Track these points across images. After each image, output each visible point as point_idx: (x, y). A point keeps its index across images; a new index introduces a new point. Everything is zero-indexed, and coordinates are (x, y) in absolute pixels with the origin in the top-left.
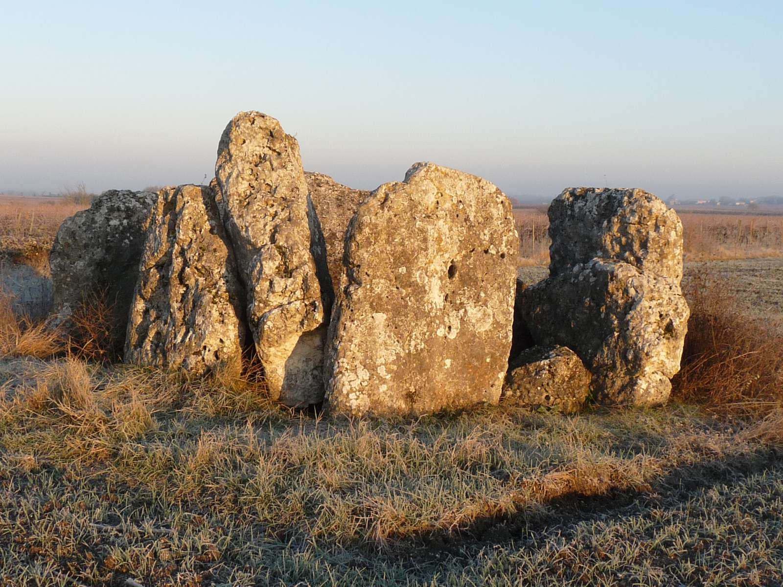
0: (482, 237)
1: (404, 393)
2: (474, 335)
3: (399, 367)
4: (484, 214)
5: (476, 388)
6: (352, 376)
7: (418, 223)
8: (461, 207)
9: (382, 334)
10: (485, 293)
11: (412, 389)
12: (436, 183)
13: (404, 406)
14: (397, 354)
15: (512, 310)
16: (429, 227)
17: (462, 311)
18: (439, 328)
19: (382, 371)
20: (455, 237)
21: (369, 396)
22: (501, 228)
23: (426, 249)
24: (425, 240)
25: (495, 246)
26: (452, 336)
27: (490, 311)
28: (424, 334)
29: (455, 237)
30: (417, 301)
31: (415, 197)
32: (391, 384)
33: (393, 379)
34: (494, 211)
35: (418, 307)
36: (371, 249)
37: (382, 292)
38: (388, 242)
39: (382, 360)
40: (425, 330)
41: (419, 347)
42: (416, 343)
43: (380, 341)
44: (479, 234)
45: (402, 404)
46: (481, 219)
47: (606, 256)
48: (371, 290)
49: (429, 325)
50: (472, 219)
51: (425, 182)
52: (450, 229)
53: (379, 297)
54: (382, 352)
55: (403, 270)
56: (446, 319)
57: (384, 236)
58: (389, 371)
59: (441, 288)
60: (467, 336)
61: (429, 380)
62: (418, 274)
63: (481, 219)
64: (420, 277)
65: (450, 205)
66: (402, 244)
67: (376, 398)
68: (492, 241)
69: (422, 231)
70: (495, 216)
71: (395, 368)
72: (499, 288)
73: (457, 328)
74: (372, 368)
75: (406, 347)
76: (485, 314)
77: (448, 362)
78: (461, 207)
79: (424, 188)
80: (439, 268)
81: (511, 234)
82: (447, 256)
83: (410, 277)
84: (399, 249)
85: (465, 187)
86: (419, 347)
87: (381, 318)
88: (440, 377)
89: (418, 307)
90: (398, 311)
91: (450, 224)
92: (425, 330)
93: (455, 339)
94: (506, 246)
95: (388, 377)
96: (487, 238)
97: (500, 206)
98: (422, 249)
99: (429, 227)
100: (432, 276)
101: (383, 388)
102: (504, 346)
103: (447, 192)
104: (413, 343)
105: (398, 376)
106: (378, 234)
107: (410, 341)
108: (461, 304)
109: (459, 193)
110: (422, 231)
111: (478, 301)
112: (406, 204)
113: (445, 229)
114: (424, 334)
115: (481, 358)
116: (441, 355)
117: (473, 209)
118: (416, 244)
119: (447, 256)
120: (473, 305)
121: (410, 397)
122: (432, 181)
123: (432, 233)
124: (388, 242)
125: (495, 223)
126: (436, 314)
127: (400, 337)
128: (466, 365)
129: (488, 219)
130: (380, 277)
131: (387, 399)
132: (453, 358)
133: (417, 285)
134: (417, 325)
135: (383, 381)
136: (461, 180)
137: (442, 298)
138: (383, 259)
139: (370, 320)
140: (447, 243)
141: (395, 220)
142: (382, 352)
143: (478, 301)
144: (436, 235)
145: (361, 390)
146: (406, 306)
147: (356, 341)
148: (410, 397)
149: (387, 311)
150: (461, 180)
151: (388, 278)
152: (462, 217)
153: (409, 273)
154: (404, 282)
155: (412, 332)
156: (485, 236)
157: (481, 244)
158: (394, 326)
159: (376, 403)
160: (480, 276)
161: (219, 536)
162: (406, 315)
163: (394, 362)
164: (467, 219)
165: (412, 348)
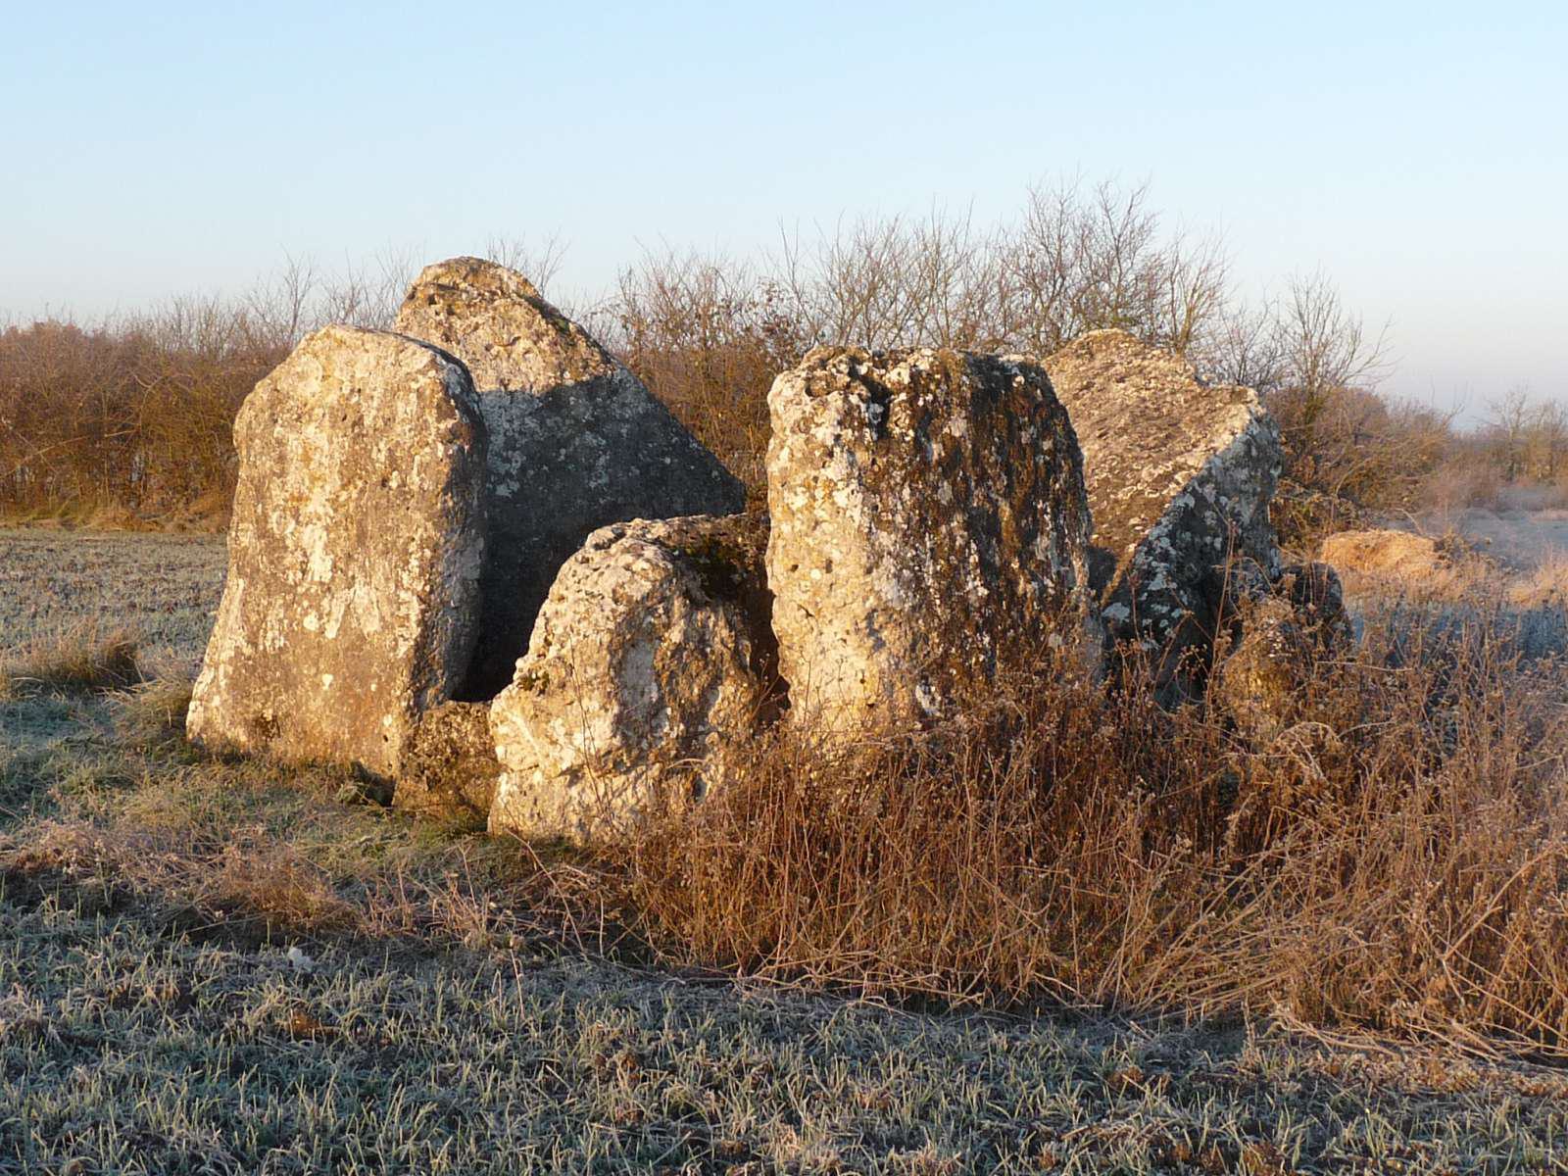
1: (251, 717)
7: (278, 429)
8: (354, 399)
11: (268, 715)
13: (243, 738)
15: (414, 610)
16: (292, 436)
18: (306, 614)
22: (407, 440)
23: (282, 474)
24: (282, 459)
30: (272, 562)
31: (283, 386)
35: (274, 575)
40: (281, 616)
44: (371, 450)
45: (241, 735)
49: (287, 606)
50: (368, 421)
56: (325, 603)
59: (326, 546)
65: (336, 397)
68: (393, 462)
69: (280, 442)
70: (400, 415)
77: (327, 679)
78: (354, 399)
79: (299, 369)
80: (321, 510)
81: (427, 450)
85: (373, 363)
88: (316, 704)
89: (274, 575)
91: (328, 430)
92: (281, 616)
93: (336, 639)
94: (419, 474)
96: (382, 457)
97: (413, 397)
98: (274, 474)
99: (292, 436)
100: (309, 522)
103: (337, 374)
104: (270, 635)
107: (266, 631)
109: (358, 375)
110: (280, 442)
113: (322, 440)
116: (316, 664)
117: (375, 404)
118: (268, 465)
121: (262, 727)
122: (315, 355)
123: (294, 447)
125: (398, 429)
126: (308, 590)
132: (334, 674)
134: (270, 603)
136: (367, 351)
137: (329, 564)
148: (262, 727)
150: (367, 351)
161: (1075, 1122)
165: (268, 644)
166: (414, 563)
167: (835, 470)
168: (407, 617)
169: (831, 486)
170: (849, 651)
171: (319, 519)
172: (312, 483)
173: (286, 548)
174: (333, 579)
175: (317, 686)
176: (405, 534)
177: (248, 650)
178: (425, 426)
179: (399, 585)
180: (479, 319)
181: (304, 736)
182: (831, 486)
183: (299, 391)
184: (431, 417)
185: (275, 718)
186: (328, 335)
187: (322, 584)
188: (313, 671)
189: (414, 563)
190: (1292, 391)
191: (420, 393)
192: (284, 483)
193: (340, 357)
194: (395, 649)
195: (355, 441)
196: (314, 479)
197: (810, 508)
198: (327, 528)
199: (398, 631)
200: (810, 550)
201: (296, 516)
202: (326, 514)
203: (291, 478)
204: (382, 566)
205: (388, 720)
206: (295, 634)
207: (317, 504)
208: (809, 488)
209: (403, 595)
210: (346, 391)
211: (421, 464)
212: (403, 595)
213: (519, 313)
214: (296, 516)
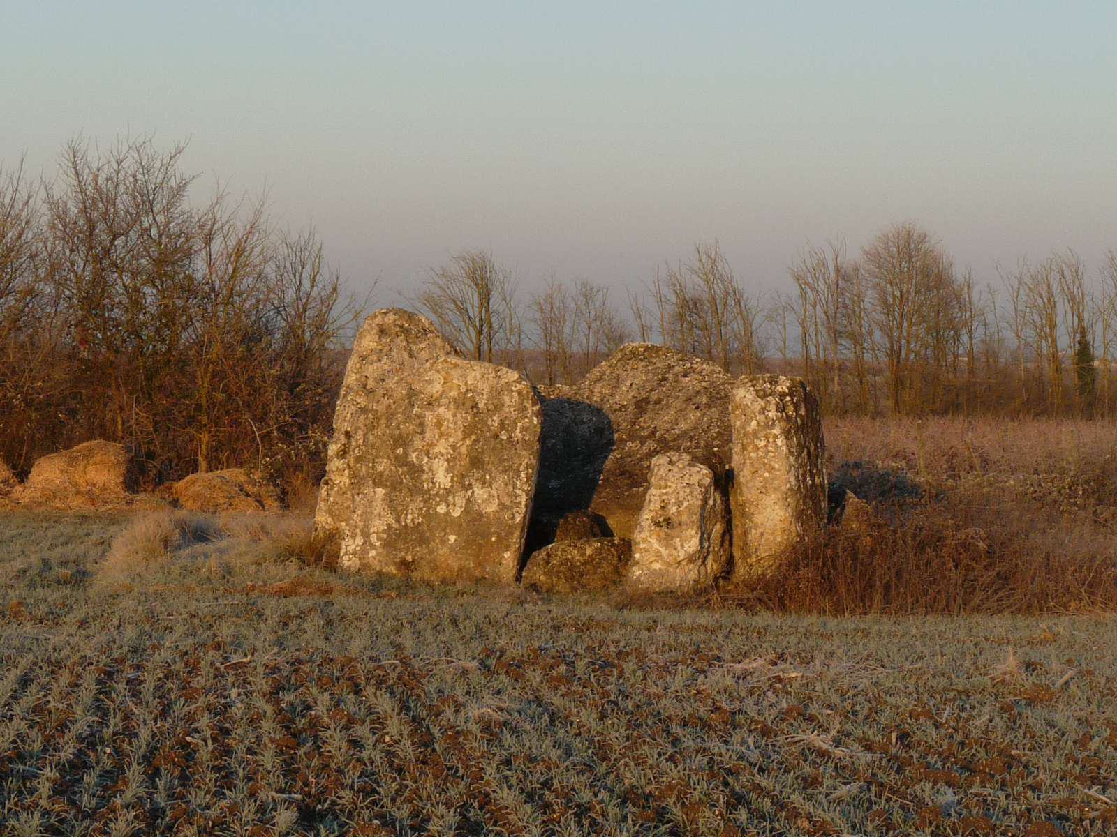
0: (490, 423)
2: (481, 515)
3: (389, 536)
4: (495, 402)
5: (479, 565)
6: (351, 541)
9: (379, 507)
10: (490, 475)
11: (409, 558)
12: (443, 373)
14: (388, 525)
17: (470, 492)
18: (439, 505)
19: (373, 538)
20: (460, 423)
21: (360, 559)
23: (422, 432)
24: (422, 424)
25: (507, 431)
26: (456, 513)
27: (494, 493)
28: (421, 509)
29: (460, 423)
30: (412, 479)
31: (416, 386)
32: (380, 550)
33: (383, 546)
34: (507, 399)
36: (375, 432)
37: (385, 470)
38: (387, 426)
39: (375, 529)
41: (416, 521)
42: (412, 516)
43: (376, 512)
46: (491, 407)
47: (432, 489)
48: (373, 467)
49: (425, 502)
50: (481, 406)
51: (430, 373)
52: (454, 416)
53: (381, 474)
54: (376, 522)
55: (400, 451)
57: (383, 421)
58: (379, 539)
60: (473, 517)
61: (430, 552)
62: (414, 455)
63: (491, 407)
64: (417, 458)
66: (398, 428)
67: (366, 561)
68: (502, 426)
71: (385, 536)
72: (505, 471)
73: (461, 507)
74: (366, 536)
75: (402, 520)
76: (490, 496)
77: (452, 538)
80: (444, 451)
82: (451, 440)
83: (406, 457)
84: (397, 432)
85: (479, 377)
86: (416, 521)
87: (381, 492)
90: (394, 486)
95: (378, 544)
101: (373, 553)
102: (511, 528)
104: (410, 517)
105: (388, 544)
106: (378, 419)
107: (406, 515)
108: (470, 485)
111: (484, 483)
112: (404, 392)
113: (449, 415)
114: (421, 509)
115: (486, 536)
116: (444, 530)
119: (451, 440)
120: (480, 487)
124: (387, 426)
127: (393, 509)
128: (469, 543)
129: (499, 407)
130: (383, 457)
131: (376, 563)
133: (414, 464)
135: (373, 547)
138: (385, 441)
139: (372, 494)
140: (449, 427)
141: (393, 406)
142: (376, 522)
143: (484, 483)
144: (435, 420)
145: (354, 554)
146: (402, 482)
147: (359, 512)
149: (387, 486)
151: (388, 458)
152: (468, 404)
153: (406, 454)
154: (402, 461)
155: (408, 507)
156: (495, 422)
157: (489, 430)
158: (389, 500)
159: (365, 566)
160: (487, 459)
162: (400, 491)
163: (384, 531)
164: (475, 406)
165: (408, 522)
166: (523, 476)
167: (776, 431)
168: (520, 503)
169: (775, 436)
170: (777, 507)
171: (442, 455)
172: (440, 437)
173: (423, 471)
174: (452, 486)
175: (444, 541)
176: (517, 461)
177: (395, 525)
178: (525, 409)
179: (514, 487)
180: (422, 345)
181: (435, 568)
182: (775, 436)
183: (428, 390)
184: (528, 404)
185: (413, 561)
186: (446, 361)
187: (445, 489)
188: (443, 534)
189: (523, 476)
190: (572, 513)
191: (520, 393)
192: (423, 438)
193: (455, 373)
194: (513, 518)
195: (475, 415)
196: (441, 435)
197: (766, 446)
198: (448, 460)
199: (515, 510)
200: (764, 464)
201: (427, 454)
202: (448, 453)
203: (428, 435)
204: (501, 479)
205: (507, 555)
206: (430, 516)
207: (442, 447)
208: (766, 437)
209: (518, 492)
210: (463, 390)
211: (523, 428)
212: (518, 492)
213: (439, 341)
214: (427, 454)
